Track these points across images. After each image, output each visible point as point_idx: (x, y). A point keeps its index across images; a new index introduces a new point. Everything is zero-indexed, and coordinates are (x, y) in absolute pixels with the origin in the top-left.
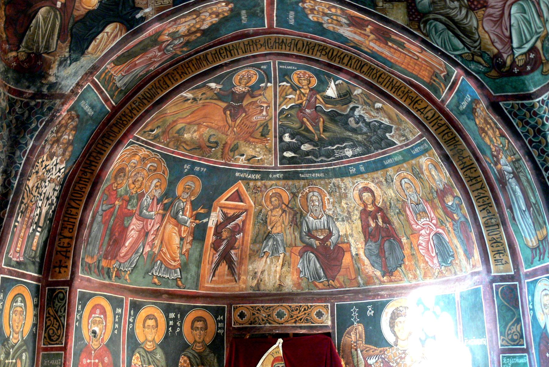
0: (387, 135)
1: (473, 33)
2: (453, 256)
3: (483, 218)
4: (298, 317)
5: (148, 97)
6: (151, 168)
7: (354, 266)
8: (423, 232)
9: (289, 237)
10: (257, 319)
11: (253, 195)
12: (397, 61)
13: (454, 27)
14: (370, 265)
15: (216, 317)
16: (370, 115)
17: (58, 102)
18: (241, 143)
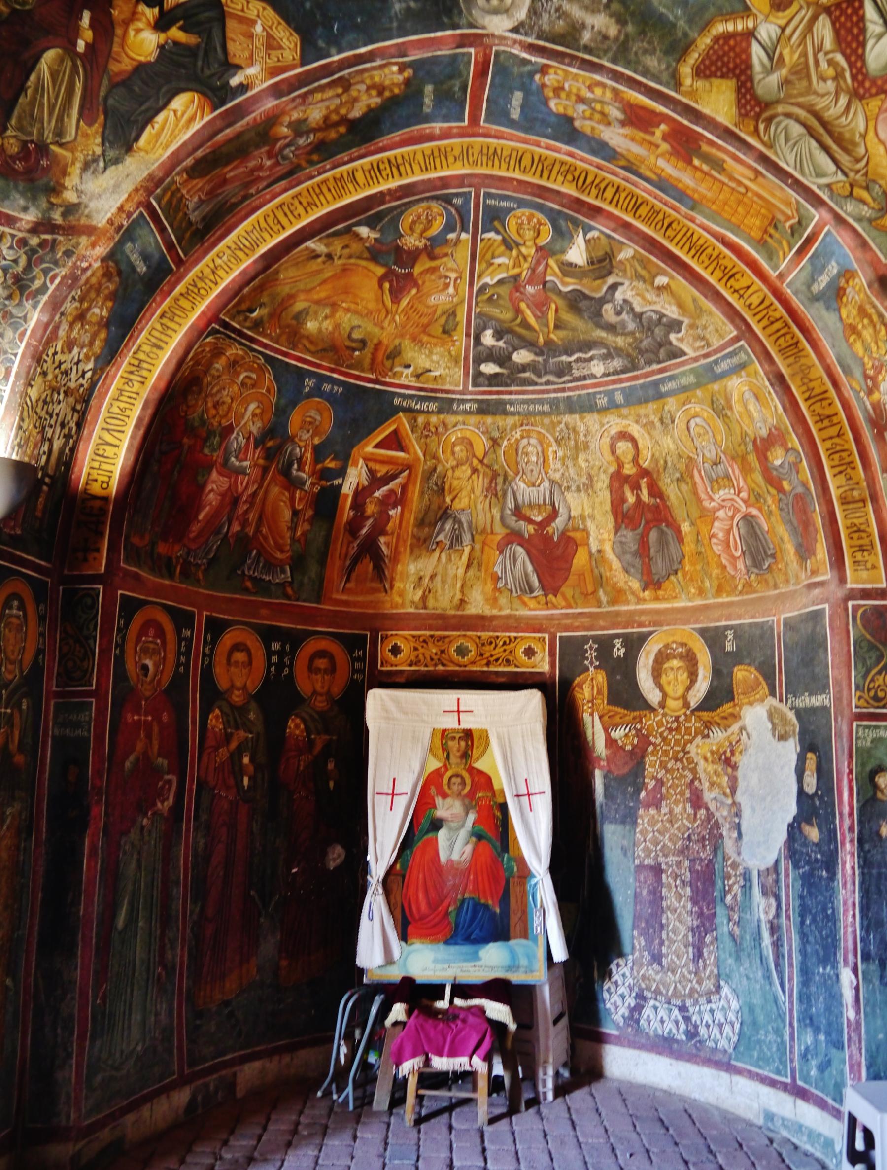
0: (673, 337)
1: (855, 145)
2: (773, 556)
4: (492, 656)
7: (592, 571)
8: (721, 514)
10: (421, 656)
11: (423, 440)
12: (705, 197)
13: (821, 130)
14: (621, 570)
15: (351, 652)
16: (644, 298)
17: (84, 240)
18: (407, 343)
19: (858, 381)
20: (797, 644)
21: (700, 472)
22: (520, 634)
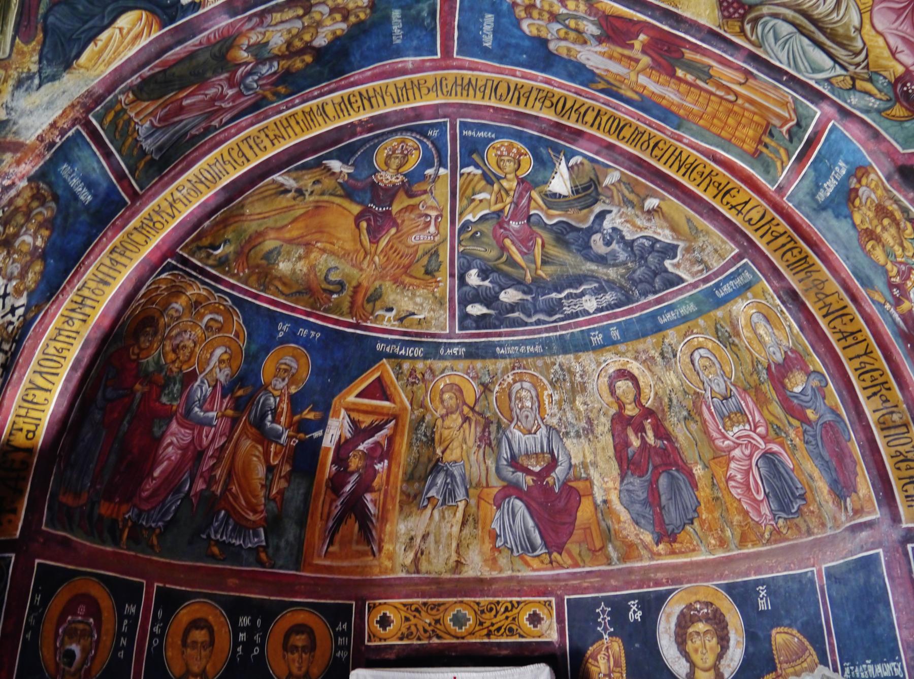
0: (668, 263)
2: (802, 497)
3: (874, 411)
4: (492, 625)
5: (206, 178)
6: (212, 323)
7: (598, 524)
8: (737, 453)
9: (475, 469)
10: (413, 628)
11: (409, 388)
13: (813, 28)
14: (630, 521)
15: (334, 626)
16: (634, 225)
19: (881, 292)
20: (847, 599)
21: (709, 409)
22: (523, 599)
